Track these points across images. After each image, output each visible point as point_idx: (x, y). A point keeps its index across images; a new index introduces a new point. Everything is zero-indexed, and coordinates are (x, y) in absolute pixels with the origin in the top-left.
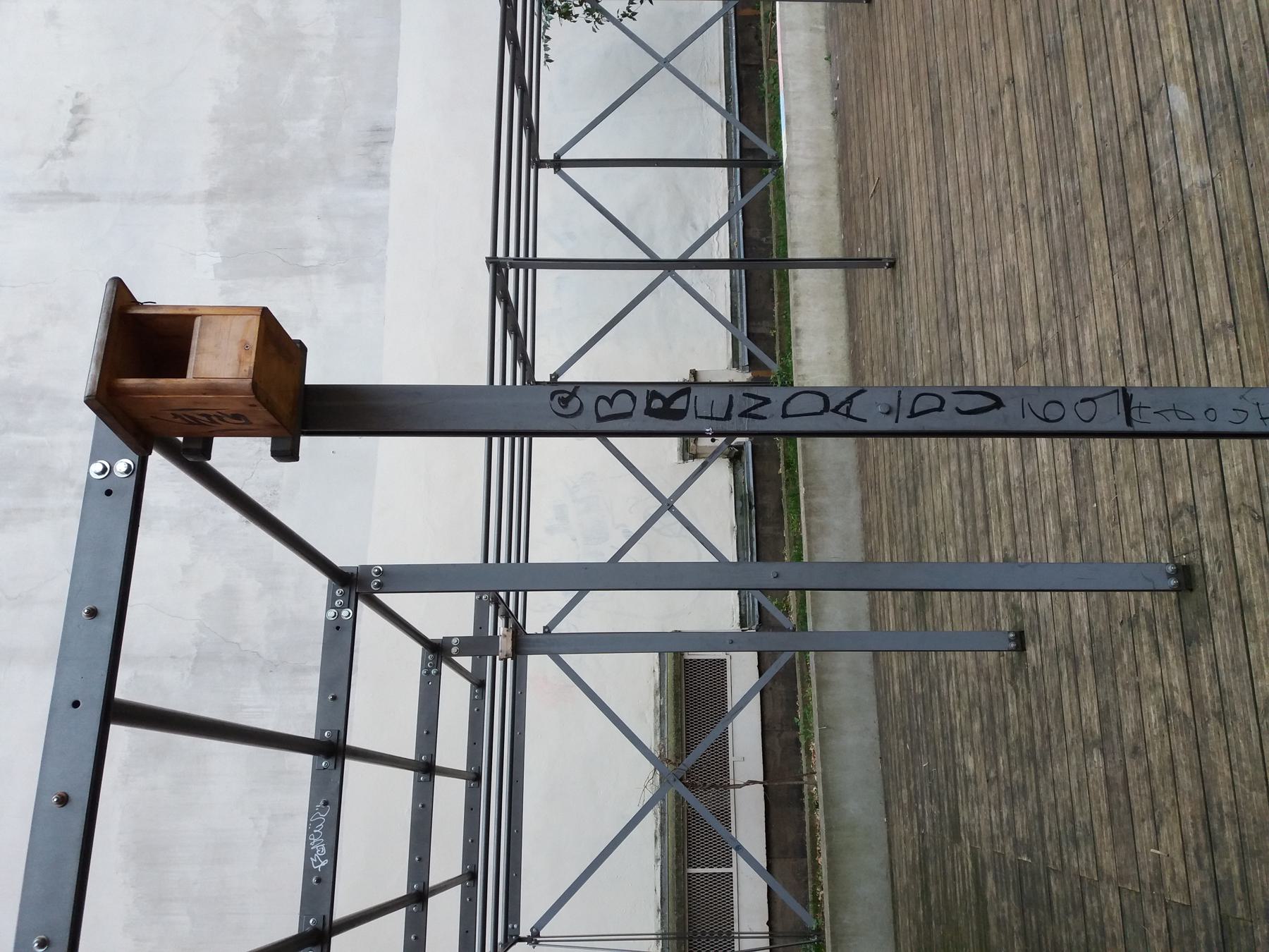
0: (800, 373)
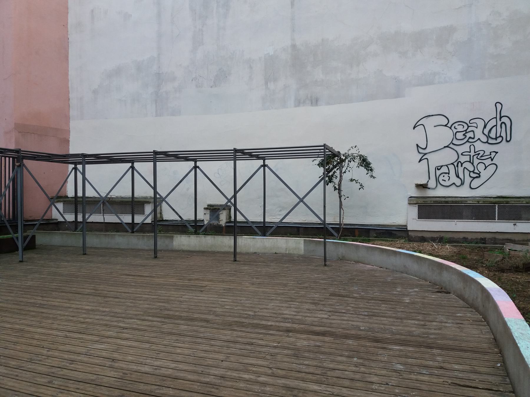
0: (178, 236)
